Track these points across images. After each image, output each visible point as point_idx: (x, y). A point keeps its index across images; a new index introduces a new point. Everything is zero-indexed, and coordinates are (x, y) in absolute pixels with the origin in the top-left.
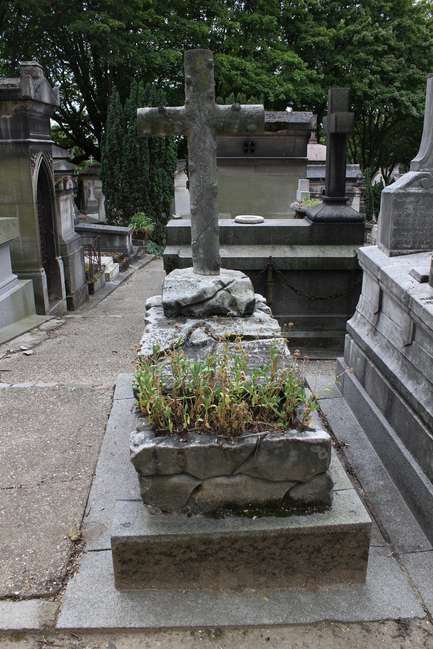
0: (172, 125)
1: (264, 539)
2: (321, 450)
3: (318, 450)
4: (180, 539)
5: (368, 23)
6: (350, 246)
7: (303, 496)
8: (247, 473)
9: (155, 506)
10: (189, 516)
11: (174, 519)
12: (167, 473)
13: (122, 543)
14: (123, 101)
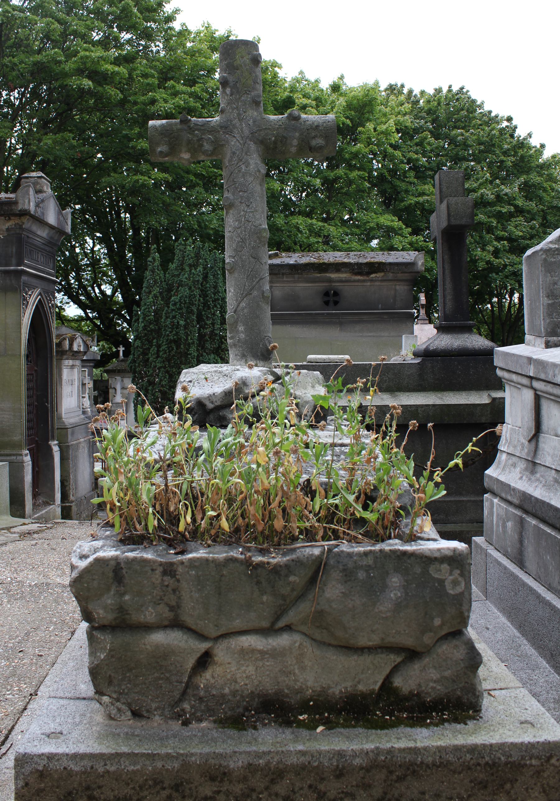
0: (198, 140)
1: (340, 773)
2: (451, 574)
3: (443, 572)
4: (159, 764)
5: (487, 179)
6: (481, 392)
7: (419, 685)
8: (303, 628)
9: (118, 700)
10: (186, 723)
11: (153, 728)
12: (142, 619)
13: (37, 770)
14: (164, 265)
